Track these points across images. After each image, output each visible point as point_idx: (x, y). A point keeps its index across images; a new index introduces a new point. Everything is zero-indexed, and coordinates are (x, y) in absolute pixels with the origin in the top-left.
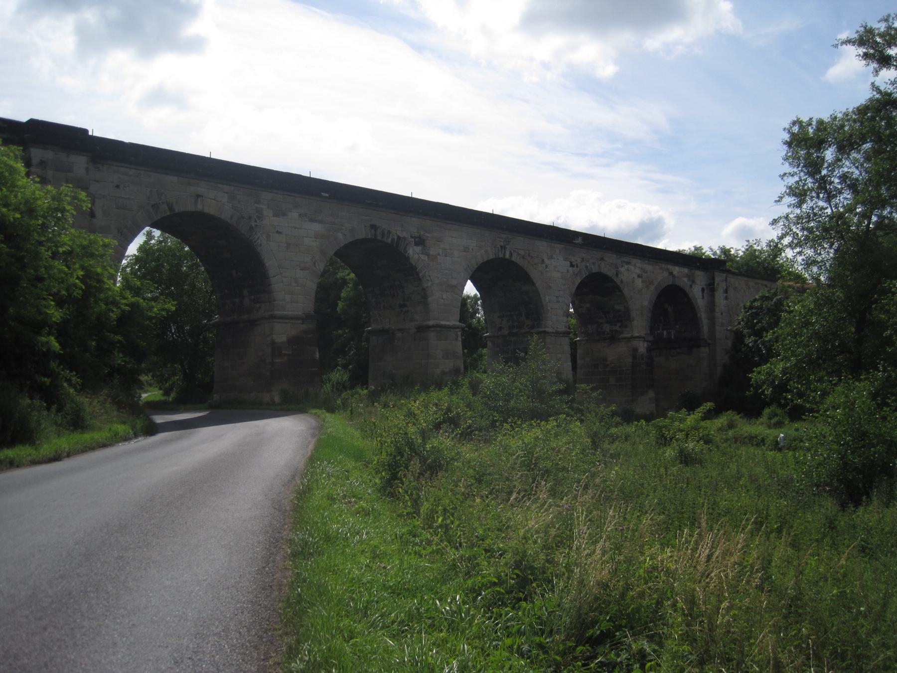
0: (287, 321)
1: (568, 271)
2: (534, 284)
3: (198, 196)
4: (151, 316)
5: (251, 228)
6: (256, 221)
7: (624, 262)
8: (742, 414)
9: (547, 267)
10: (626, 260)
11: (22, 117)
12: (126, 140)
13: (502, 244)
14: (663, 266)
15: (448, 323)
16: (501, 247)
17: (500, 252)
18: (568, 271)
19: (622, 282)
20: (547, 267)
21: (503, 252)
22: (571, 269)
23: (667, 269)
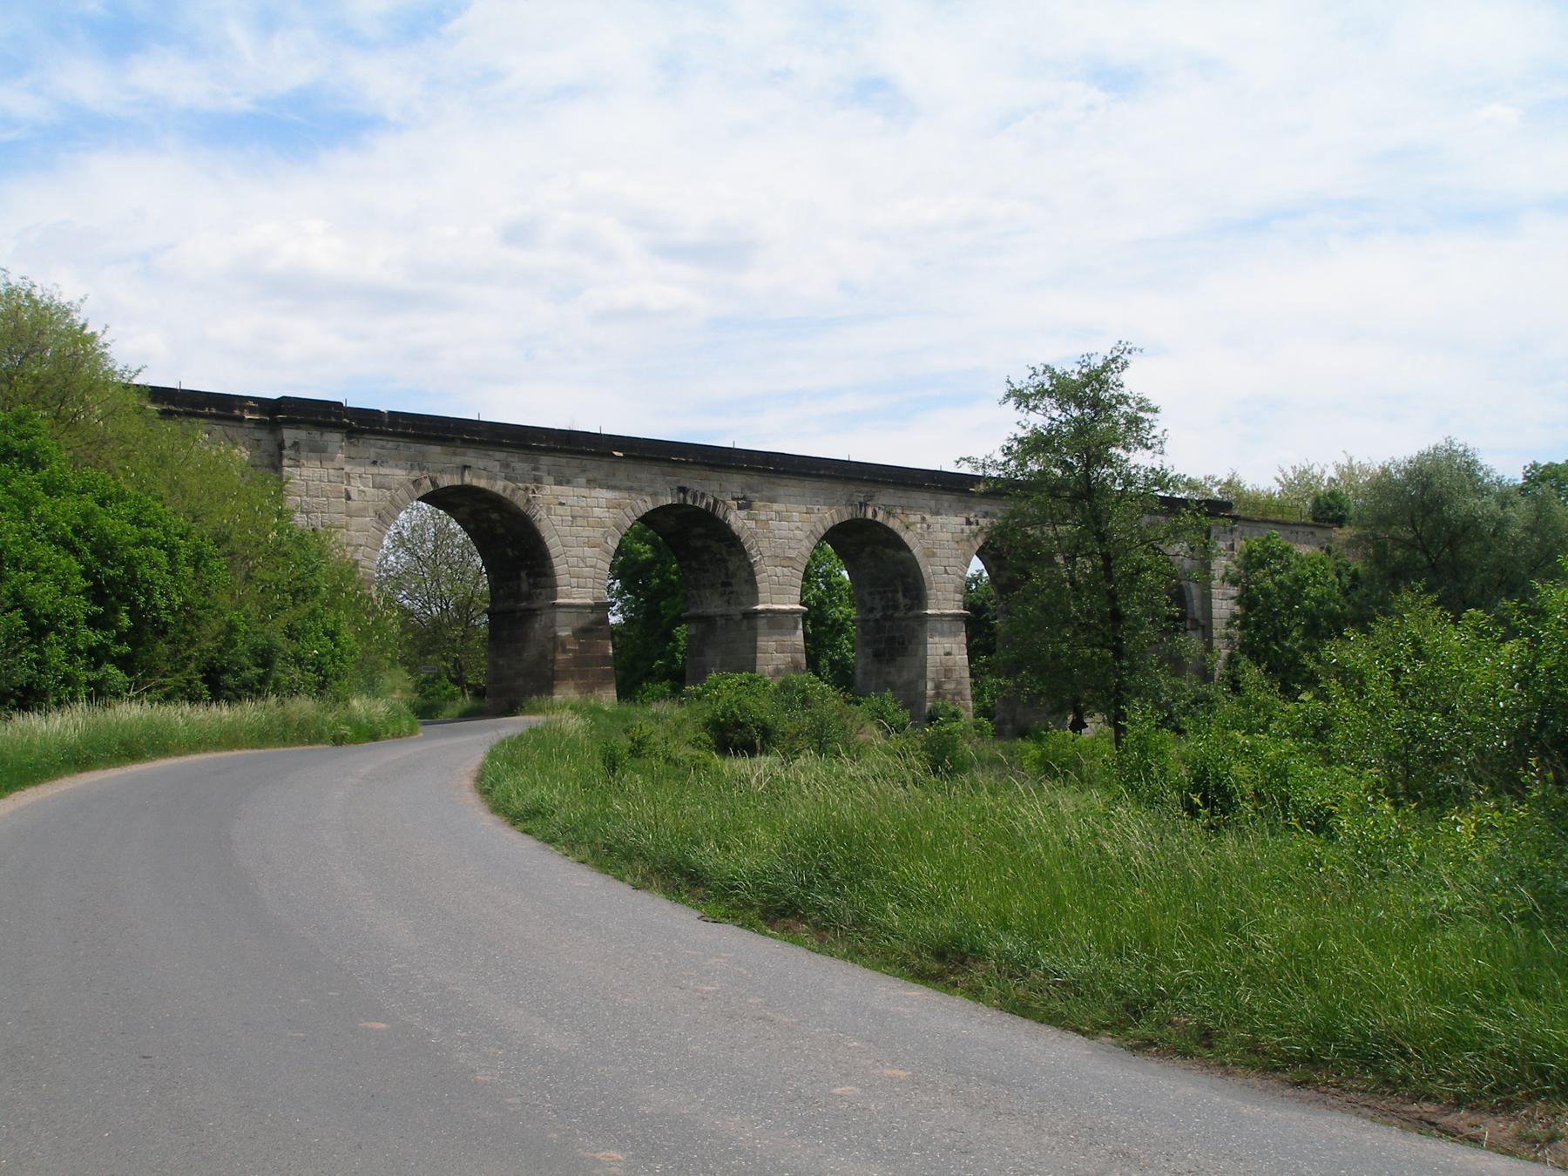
18: (962, 530)
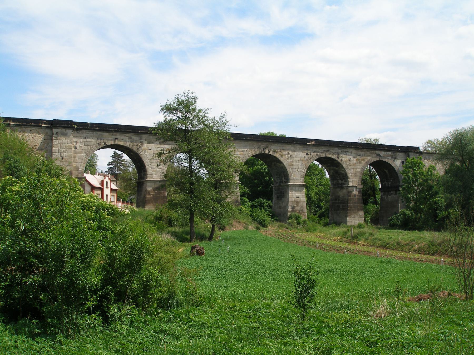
0: (153, 182)
1: (305, 157)
2: (283, 164)
3: (116, 139)
4: (273, 190)
5: (138, 149)
6: (140, 146)
7: (344, 151)
8: (412, 230)
9: (291, 156)
10: (345, 150)
11: (257, 133)
12: (30, 118)
13: (264, 147)
14: (372, 152)
15: (153, 179)
16: (263, 149)
17: (262, 151)
18: (305, 157)
19: (341, 160)
20: (291, 156)
21: (264, 151)
22: (306, 156)
23: (376, 153)
